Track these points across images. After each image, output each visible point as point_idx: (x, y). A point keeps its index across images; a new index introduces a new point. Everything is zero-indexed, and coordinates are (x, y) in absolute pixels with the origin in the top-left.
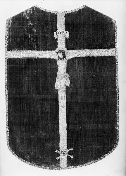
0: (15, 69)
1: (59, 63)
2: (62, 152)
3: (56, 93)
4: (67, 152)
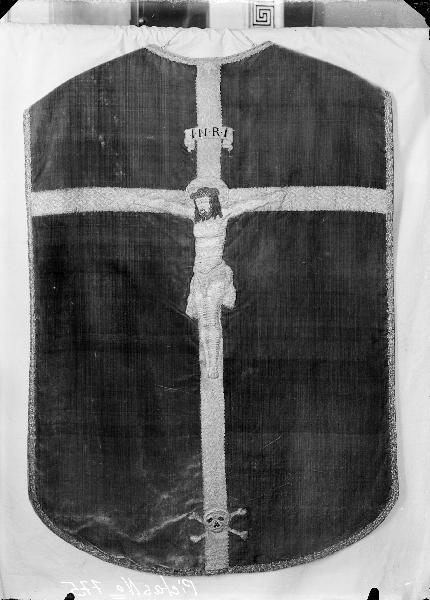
0: (59, 252)
1: (199, 229)
2: (211, 519)
3: (188, 330)
4: (227, 521)
